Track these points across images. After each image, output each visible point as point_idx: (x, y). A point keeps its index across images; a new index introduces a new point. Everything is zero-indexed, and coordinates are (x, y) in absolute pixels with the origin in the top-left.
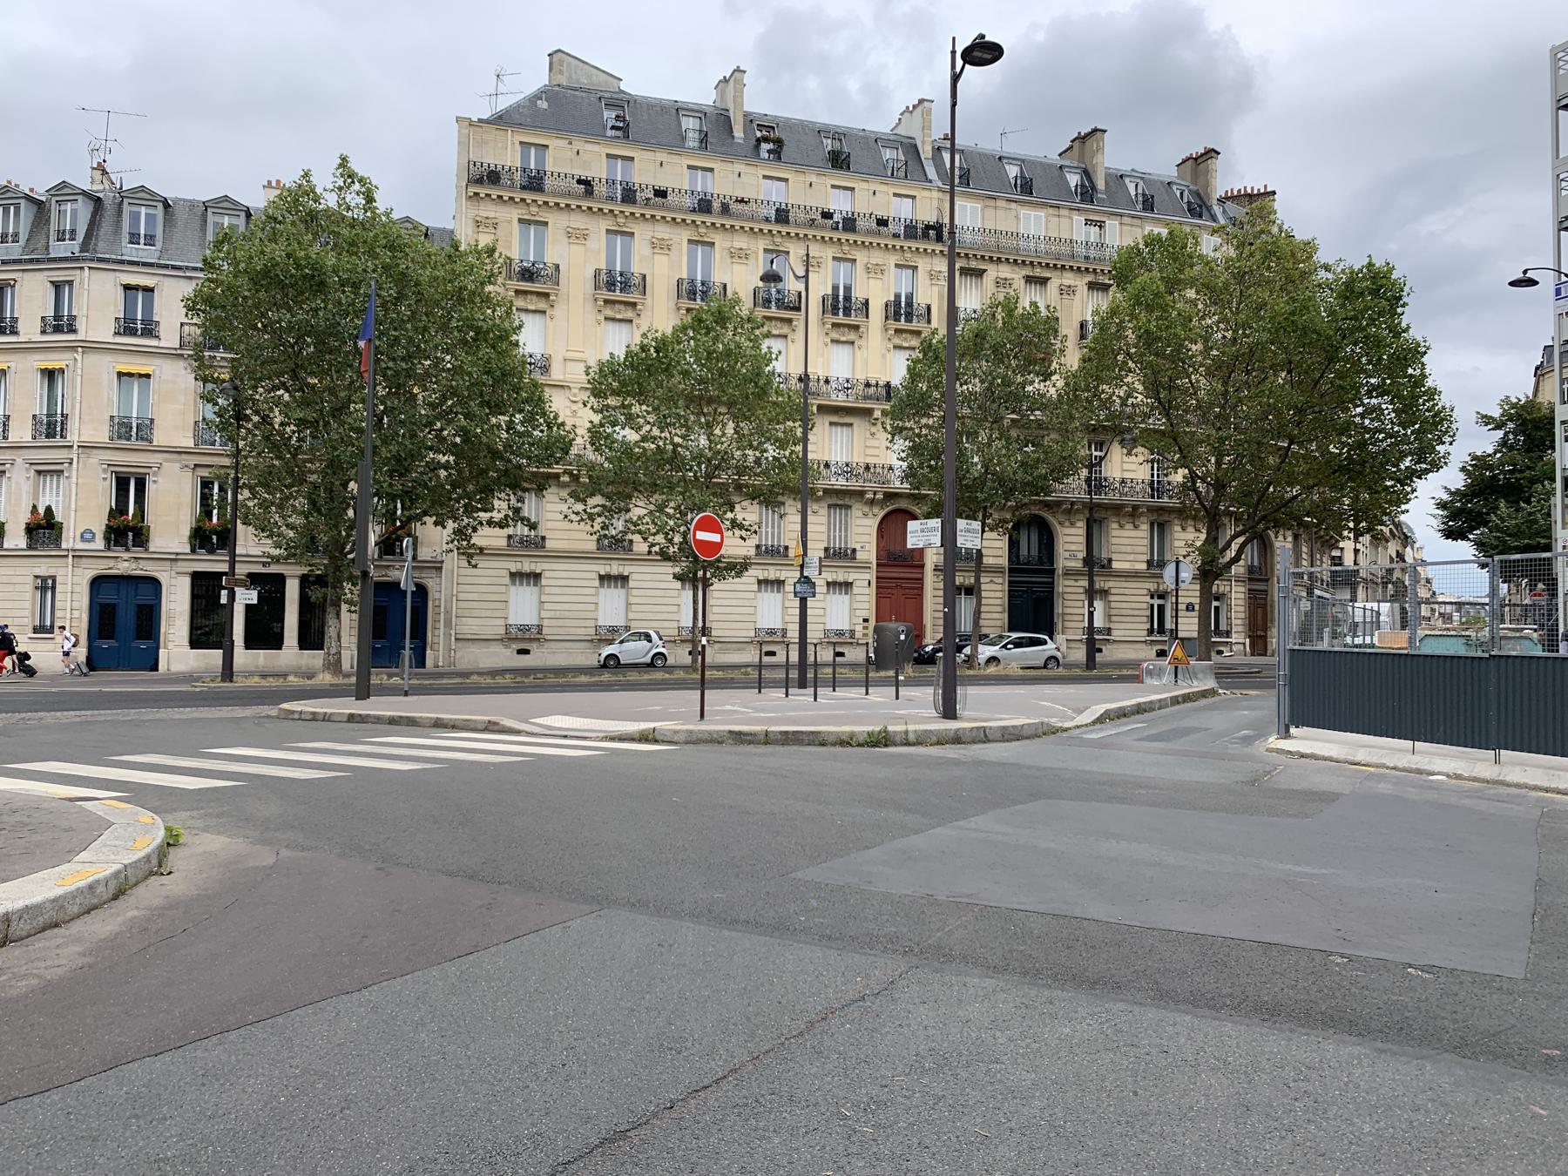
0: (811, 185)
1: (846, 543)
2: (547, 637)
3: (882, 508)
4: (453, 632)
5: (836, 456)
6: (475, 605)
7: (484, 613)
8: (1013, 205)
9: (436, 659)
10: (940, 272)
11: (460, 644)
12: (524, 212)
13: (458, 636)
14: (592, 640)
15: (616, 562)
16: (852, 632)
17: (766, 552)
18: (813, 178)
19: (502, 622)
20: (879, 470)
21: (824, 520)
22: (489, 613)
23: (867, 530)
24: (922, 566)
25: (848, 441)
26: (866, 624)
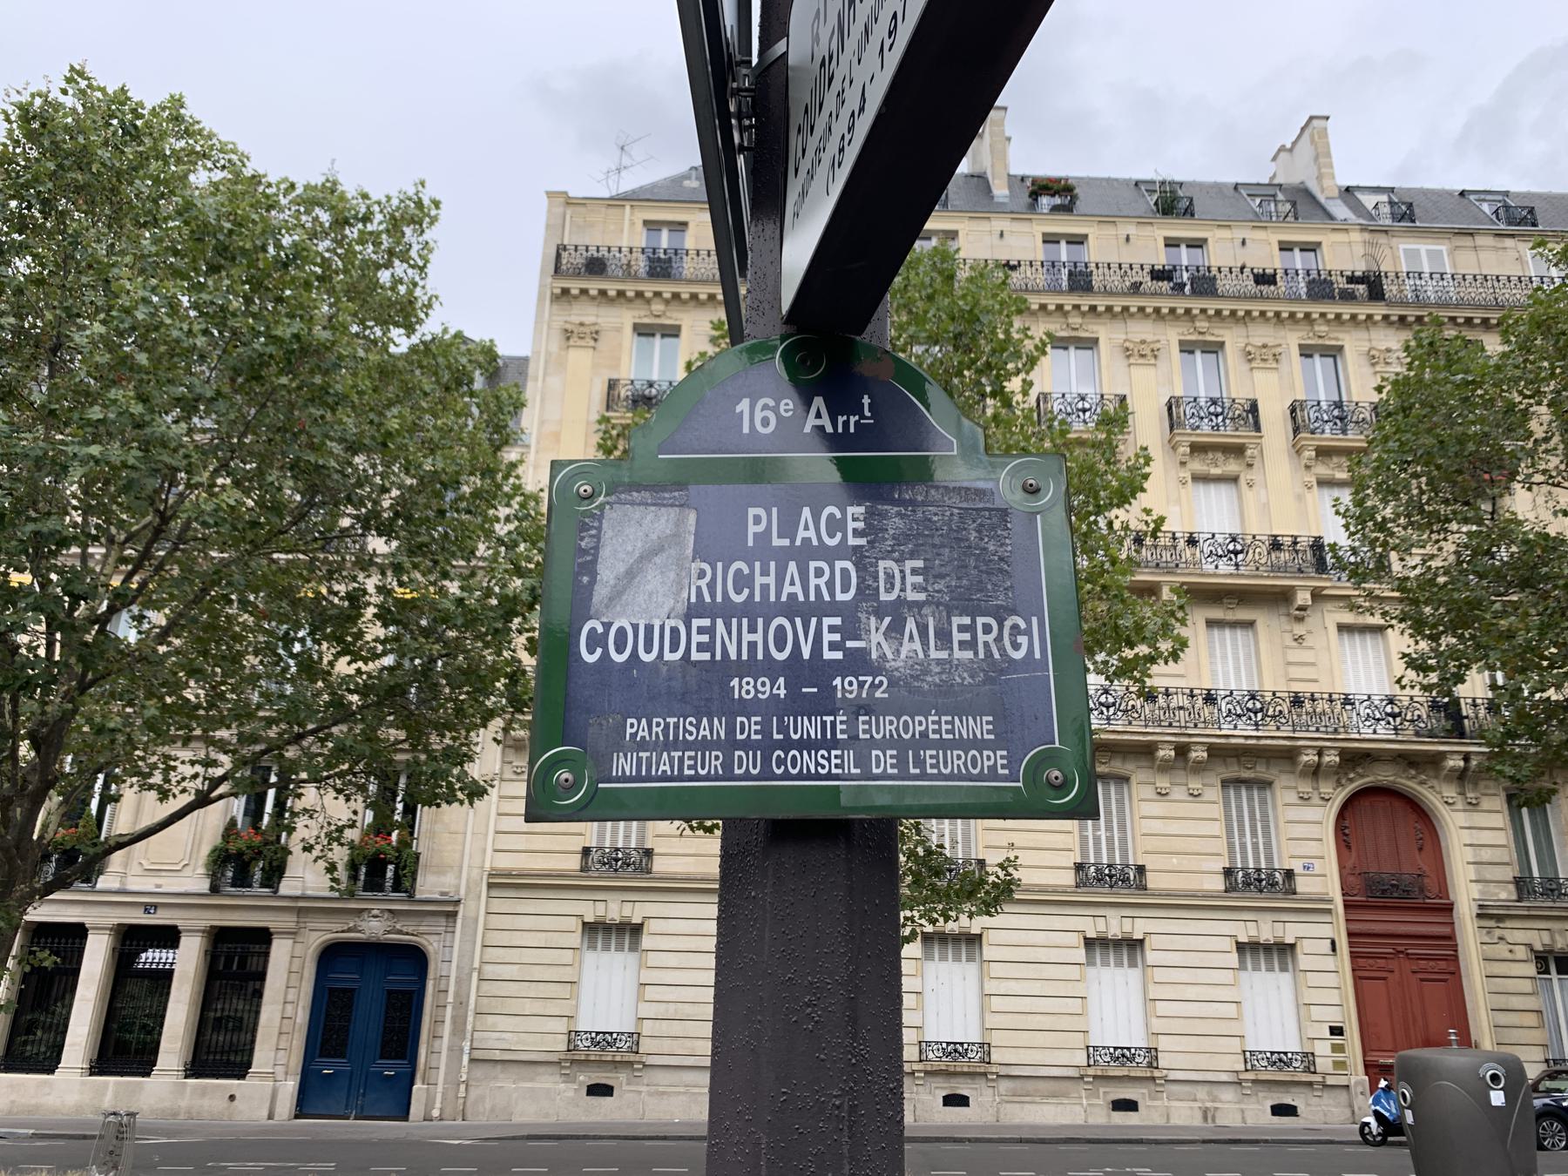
0: (1128, 239)
1: (1269, 858)
2: (651, 1060)
3: (1339, 784)
4: (467, 1046)
5: (1226, 680)
6: (512, 989)
7: (529, 1007)
8: (1509, 242)
9: (429, 1105)
10: (1389, 350)
11: (480, 1071)
12: (643, 313)
13: (478, 1054)
14: (1239, 1083)
15: (1269, 917)
16: (1309, 1058)
17: (1247, 884)
18: (1131, 230)
19: (561, 1026)
20: (1321, 706)
21: (1217, 810)
22: (537, 1007)
23: (1314, 831)
24: (1448, 909)
25: (1248, 656)
26: (1337, 1040)
